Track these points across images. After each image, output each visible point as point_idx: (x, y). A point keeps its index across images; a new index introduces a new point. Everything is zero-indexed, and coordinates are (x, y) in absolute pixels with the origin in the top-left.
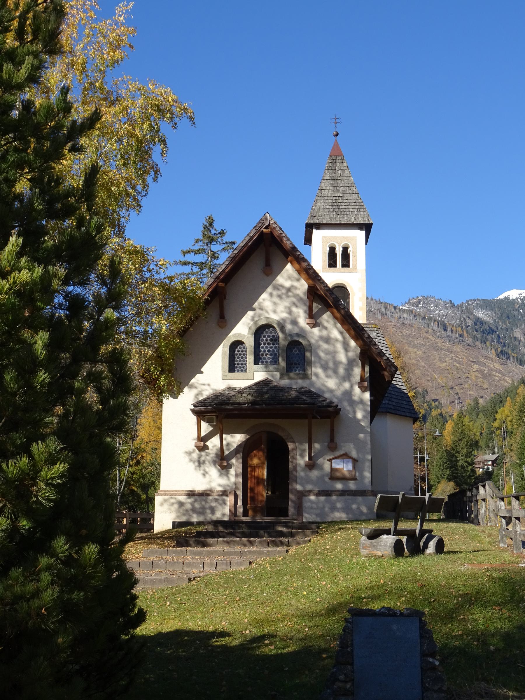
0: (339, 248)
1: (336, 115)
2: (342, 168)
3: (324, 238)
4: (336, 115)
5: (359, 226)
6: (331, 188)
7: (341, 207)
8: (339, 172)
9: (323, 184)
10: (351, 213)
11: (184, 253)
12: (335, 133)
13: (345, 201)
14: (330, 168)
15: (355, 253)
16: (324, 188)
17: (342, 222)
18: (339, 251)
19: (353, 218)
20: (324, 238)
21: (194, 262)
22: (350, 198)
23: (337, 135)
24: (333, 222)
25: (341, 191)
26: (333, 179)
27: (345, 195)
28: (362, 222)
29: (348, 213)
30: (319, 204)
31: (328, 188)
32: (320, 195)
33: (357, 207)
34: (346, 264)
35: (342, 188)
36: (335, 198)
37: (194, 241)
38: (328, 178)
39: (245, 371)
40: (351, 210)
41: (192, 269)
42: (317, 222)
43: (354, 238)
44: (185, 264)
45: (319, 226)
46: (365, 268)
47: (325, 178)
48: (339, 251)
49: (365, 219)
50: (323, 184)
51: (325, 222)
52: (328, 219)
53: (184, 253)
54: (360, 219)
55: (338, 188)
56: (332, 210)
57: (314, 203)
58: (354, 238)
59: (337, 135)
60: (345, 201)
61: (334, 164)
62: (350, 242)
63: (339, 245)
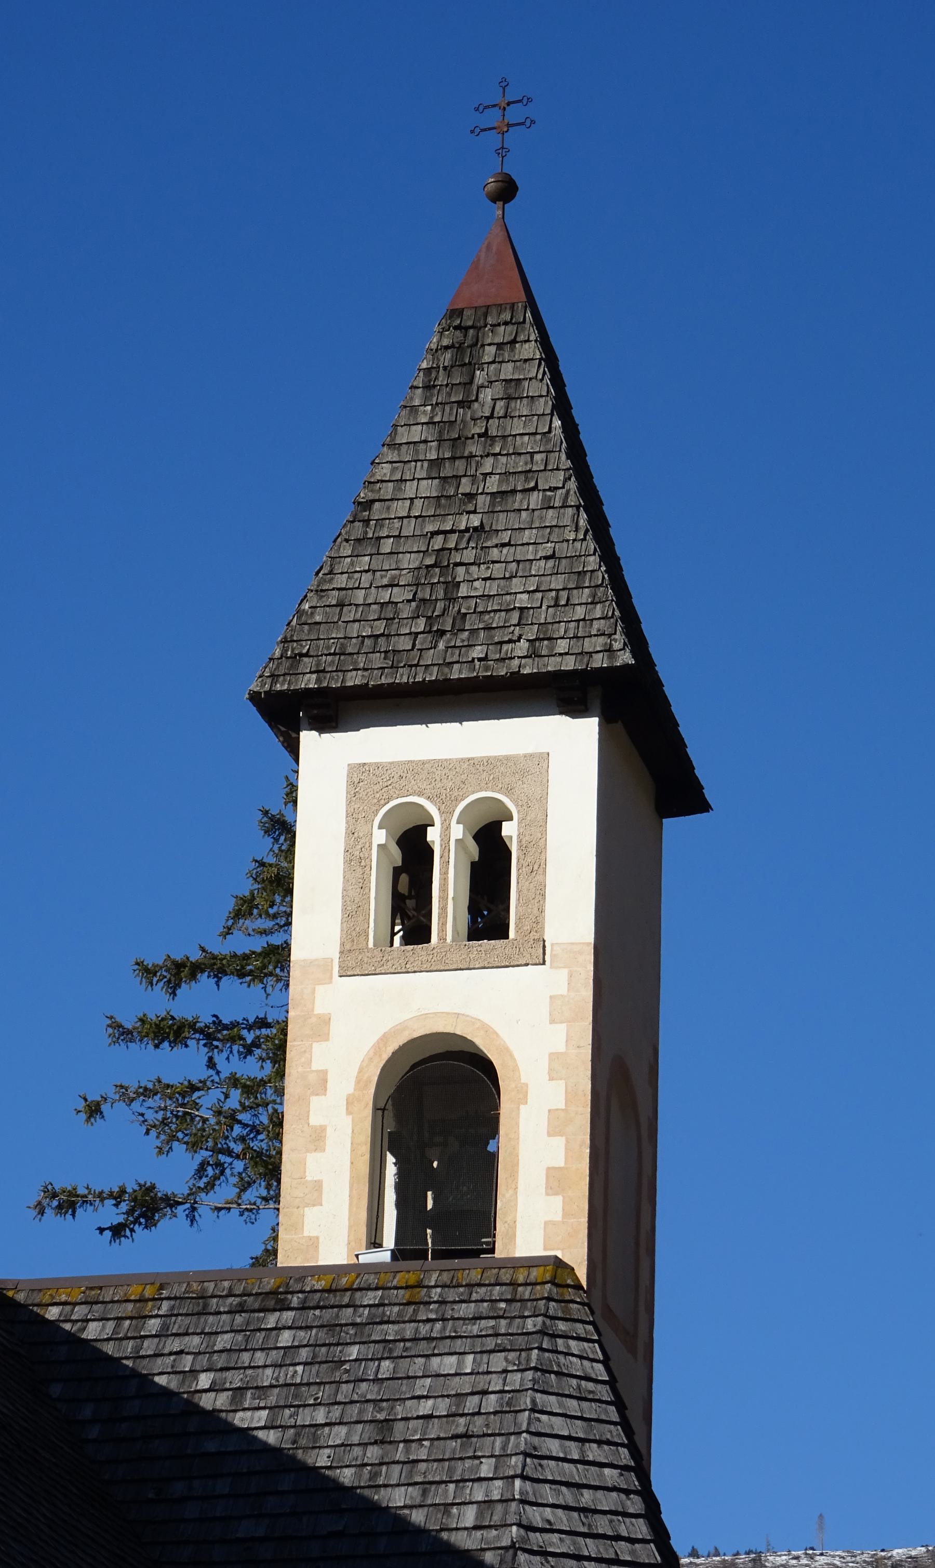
0: (446, 829)
1: (504, 85)
2: (508, 371)
3: (362, 779)
4: (504, 85)
5: (562, 693)
6: (429, 488)
7: (463, 591)
8: (487, 395)
9: (384, 471)
10: (515, 617)
11: (180, 973)
12: (491, 184)
13: (495, 554)
14: (442, 379)
15: (536, 846)
16: (388, 490)
17: (456, 673)
18: (449, 842)
19: (522, 647)
20: (362, 779)
21: (218, 1022)
22: (527, 536)
23: (506, 191)
24: (403, 677)
25: (482, 502)
26: (453, 440)
27: (501, 521)
28: (569, 664)
29: (497, 620)
30: (341, 581)
31: (410, 490)
32: (358, 530)
33: (557, 582)
34: (489, 913)
35: (493, 485)
36: (438, 542)
37: (231, 905)
38: (416, 433)
39: (547, 1194)
40: (523, 600)
41: (211, 1064)
42: (310, 682)
43: (536, 765)
44: (169, 1032)
45: (336, 709)
46: (590, 938)
47: (403, 436)
48: (449, 842)
49: (588, 645)
50: (384, 471)
51: (354, 679)
52: (377, 660)
53: (180, 973)
54: (562, 646)
55: (466, 486)
56: (406, 611)
57: (313, 583)
58: (536, 765)
59: (506, 191)
60: (495, 554)
61: (465, 356)
62: (509, 791)
63: (446, 814)
